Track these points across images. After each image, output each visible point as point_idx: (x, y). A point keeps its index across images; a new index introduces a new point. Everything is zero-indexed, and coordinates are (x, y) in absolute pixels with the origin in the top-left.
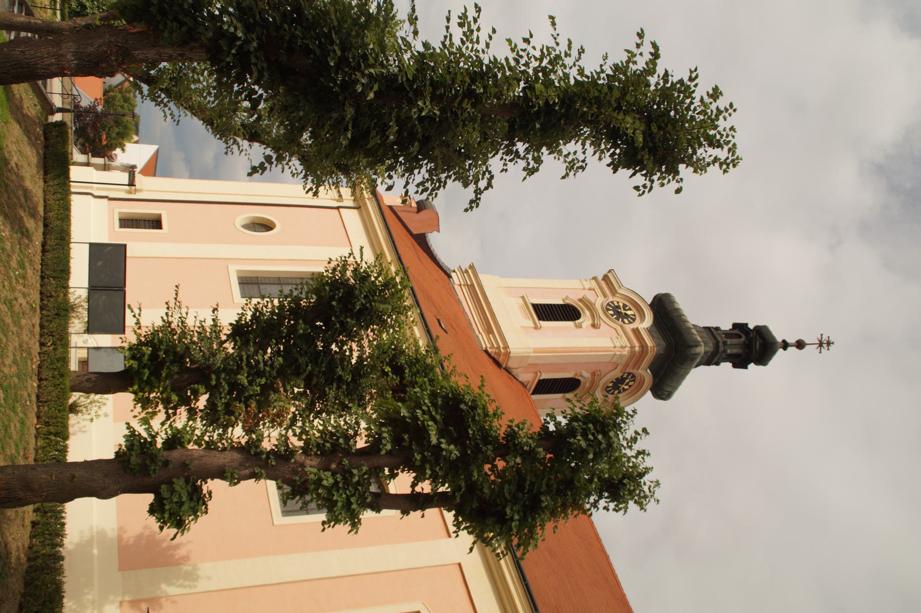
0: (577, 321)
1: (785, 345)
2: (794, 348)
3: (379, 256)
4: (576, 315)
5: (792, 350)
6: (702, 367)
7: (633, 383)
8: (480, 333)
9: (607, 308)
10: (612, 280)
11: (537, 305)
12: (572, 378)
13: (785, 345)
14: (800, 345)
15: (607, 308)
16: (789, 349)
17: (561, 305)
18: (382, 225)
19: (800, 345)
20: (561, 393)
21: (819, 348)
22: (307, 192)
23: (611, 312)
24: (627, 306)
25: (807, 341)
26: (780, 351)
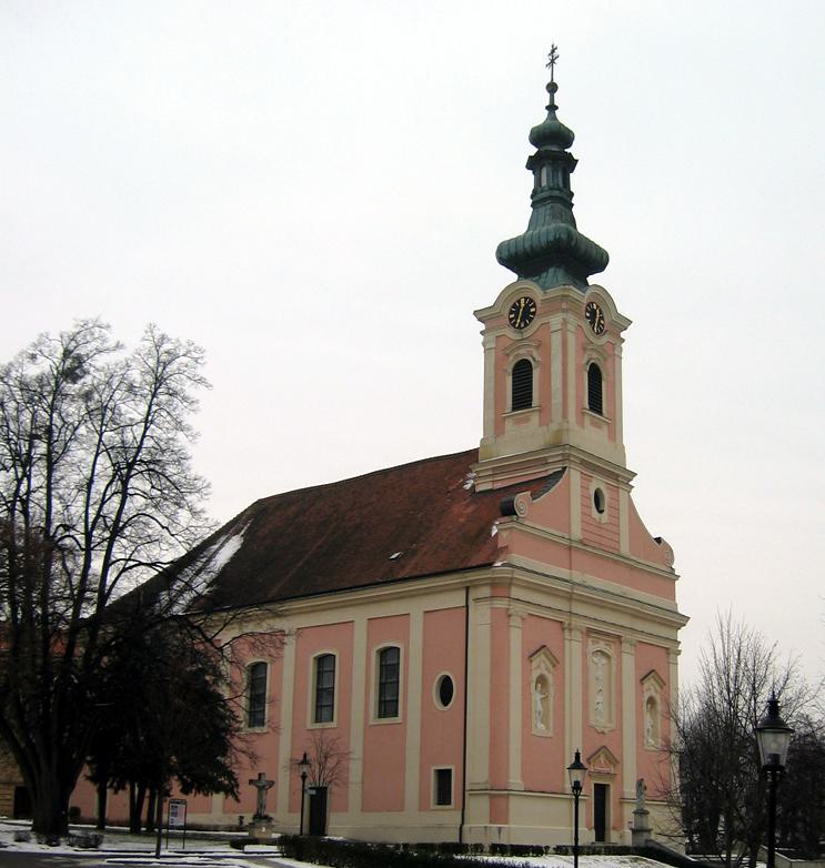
1: (552, 108)
13: (552, 108)
14: (552, 88)
18: (418, 582)
19: (552, 88)
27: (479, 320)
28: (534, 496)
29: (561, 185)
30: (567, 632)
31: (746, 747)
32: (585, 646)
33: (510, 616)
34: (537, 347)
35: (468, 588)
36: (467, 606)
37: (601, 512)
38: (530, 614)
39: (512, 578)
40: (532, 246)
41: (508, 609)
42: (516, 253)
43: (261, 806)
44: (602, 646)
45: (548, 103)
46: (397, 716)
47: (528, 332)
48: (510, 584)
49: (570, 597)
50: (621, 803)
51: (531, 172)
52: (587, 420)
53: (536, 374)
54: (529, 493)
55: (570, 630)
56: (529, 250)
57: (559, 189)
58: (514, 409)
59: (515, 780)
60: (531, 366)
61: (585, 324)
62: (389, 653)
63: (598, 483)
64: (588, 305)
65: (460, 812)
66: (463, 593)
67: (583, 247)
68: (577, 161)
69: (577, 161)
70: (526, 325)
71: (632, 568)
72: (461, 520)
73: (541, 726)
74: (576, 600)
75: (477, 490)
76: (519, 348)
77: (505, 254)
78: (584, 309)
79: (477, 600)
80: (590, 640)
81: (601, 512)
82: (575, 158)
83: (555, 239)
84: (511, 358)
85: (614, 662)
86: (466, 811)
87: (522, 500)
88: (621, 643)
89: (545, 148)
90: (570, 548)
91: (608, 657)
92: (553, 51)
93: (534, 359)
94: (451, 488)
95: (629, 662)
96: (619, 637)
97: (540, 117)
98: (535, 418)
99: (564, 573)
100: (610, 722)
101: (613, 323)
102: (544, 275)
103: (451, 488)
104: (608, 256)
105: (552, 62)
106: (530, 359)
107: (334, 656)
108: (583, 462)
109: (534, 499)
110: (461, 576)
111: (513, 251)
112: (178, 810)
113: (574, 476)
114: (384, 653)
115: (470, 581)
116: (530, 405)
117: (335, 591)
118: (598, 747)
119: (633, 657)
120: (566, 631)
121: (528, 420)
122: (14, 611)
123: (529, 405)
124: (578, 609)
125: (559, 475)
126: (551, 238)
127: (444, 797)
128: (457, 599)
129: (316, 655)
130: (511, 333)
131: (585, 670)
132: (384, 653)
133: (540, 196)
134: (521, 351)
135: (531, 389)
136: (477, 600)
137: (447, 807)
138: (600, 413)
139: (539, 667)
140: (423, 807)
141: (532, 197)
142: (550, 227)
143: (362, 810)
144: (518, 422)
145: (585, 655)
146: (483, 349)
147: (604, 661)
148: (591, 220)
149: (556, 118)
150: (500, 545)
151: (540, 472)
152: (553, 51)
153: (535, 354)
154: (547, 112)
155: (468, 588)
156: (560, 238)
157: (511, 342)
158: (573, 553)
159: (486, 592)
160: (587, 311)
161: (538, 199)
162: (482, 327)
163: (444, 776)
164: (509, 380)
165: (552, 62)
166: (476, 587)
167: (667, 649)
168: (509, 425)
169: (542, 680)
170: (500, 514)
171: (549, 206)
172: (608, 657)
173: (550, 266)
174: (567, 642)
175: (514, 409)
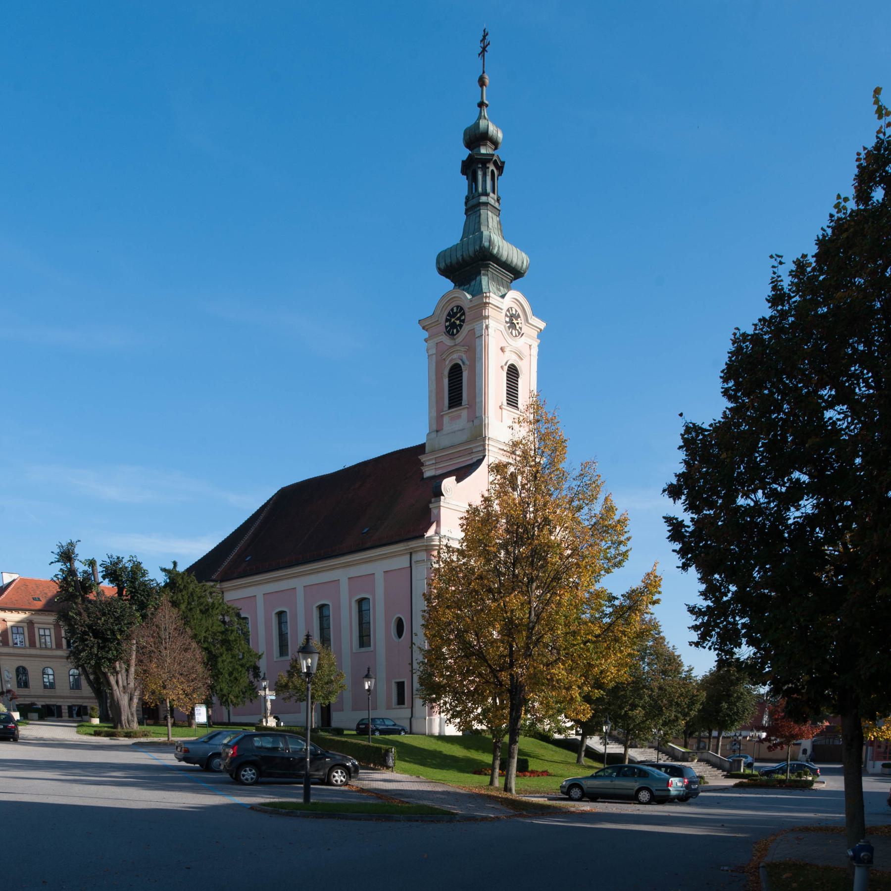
11: (449, 404)
23: (455, 331)
27: (424, 328)
28: (459, 480)
35: (411, 554)
36: (411, 567)
46: (370, 646)
47: (460, 338)
53: (465, 375)
54: (454, 478)
58: (450, 407)
62: (364, 602)
64: (508, 310)
65: (410, 709)
66: (408, 556)
70: (458, 332)
75: (425, 477)
77: (442, 265)
78: (504, 314)
86: (414, 709)
92: (484, 37)
93: (464, 363)
98: (464, 414)
105: (484, 49)
106: (461, 363)
110: (405, 544)
114: (361, 602)
117: (329, 557)
121: (459, 417)
122: (764, 503)
123: (460, 404)
127: (401, 701)
128: (404, 562)
129: (356, 599)
130: (447, 341)
132: (361, 602)
134: (455, 356)
135: (462, 390)
137: (403, 706)
141: (466, 203)
143: (343, 711)
148: (463, 181)
152: (484, 37)
153: (464, 357)
155: (411, 554)
160: (506, 315)
162: (426, 334)
163: (400, 686)
164: (446, 381)
165: (484, 49)
166: (416, 552)
168: (446, 419)
175: (450, 407)
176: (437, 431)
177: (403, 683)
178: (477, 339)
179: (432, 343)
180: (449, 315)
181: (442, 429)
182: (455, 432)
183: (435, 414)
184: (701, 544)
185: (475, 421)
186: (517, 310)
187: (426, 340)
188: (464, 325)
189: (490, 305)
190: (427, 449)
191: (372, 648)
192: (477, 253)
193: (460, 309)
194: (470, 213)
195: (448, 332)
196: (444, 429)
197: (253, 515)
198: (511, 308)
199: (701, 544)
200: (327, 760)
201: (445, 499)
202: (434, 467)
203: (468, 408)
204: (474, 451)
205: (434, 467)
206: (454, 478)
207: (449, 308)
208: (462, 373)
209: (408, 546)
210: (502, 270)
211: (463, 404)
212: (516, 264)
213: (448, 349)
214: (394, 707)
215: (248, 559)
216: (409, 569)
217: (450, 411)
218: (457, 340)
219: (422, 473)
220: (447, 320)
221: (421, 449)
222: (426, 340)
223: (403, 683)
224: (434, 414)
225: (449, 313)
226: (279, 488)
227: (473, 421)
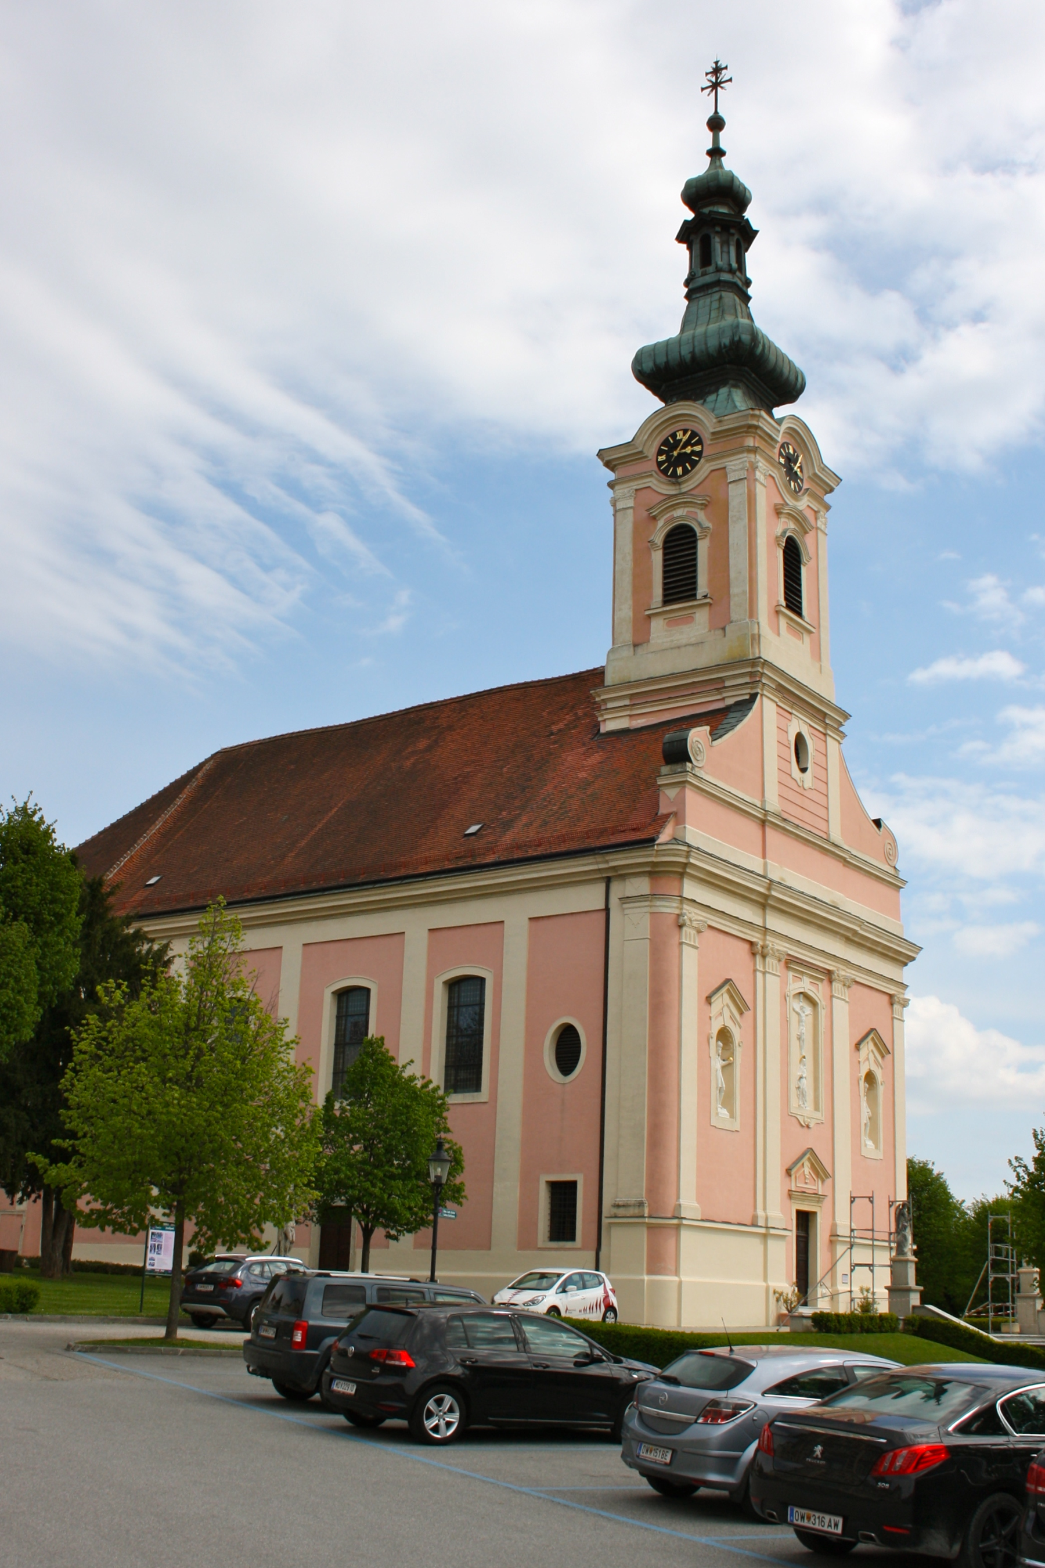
0: (698, 534)
1: (716, 153)
2: (722, 134)
3: (367, 1233)
4: (685, 532)
5: (725, 139)
6: (749, 255)
7: (790, 447)
8: (723, 699)
9: (671, 476)
10: (759, 541)
11: (665, 596)
12: (785, 552)
13: (716, 153)
14: (716, 124)
15: (671, 476)
16: (723, 145)
17: (665, 554)
18: (540, 866)
19: (716, 124)
20: (800, 568)
21: (722, 85)
22: (828, 508)
23: (680, 471)
24: (667, 439)
25: (711, 113)
26: (728, 163)
29: (735, 265)
30: (758, 958)
31: (227, 1229)
32: (784, 983)
33: (681, 927)
34: (704, 506)
36: (607, 910)
37: (804, 770)
38: (710, 927)
39: (686, 865)
40: (693, 353)
41: (678, 916)
42: (667, 363)
43: (634, 1205)
44: (805, 984)
45: (710, 146)
48: (682, 875)
49: (763, 903)
50: (831, 1242)
51: (685, 246)
52: (783, 622)
53: (703, 548)
54: (708, 728)
55: (764, 957)
56: (688, 357)
57: (731, 271)
58: (666, 602)
59: (689, 1203)
60: (695, 535)
61: (780, 474)
63: (798, 724)
65: (593, 1254)
66: (601, 887)
67: (772, 358)
68: (756, 232)
69: (756, 232)
70: (686, 472)
71: (846, 862)
72: (582, 775)
73: (724, 1112)
74: (774, 908)
75: (603, 730)
76: (674, 507)
77: (648, 366)
79: (625, 900)
80: (791, 974)
81: (804, 770)
82: (755, 228)
83: (732, 342)
84: (661, 523)
85: (823, 1013)
87: (697, 736)
88: (831, 981)
89: (706, 210)
90: (763, 823)
91: (813, 1003)
93: (700, 524)
94: (555, 728)
95: (841, 1011)
96: (829, 973)
97: (699, 167)
98: (702, 616)
99: (754, 863)
100: (817, 1108)
101: (815, 478)
102: (712, 398)
103: (555, 728)
104: (803, 379)
105: (715, 86)
107: (368, 990)
108: (781, 689)
109: (713, 740)
110: (599, 858)
111: (661, 360)
112: (163, 1241)
113: (767, 708)
114: (454, 985)
115: (614, 868)
116: (693, 597)
118: (804, 1148)
119: (889, 1269)
120: (758, 958)
121: (689, 619)
124: (776, 922)
125: (745, 705)
126: (726, 341)
128: (591, 897)
130: (664, 488)
131: (785, 1022)
132: (454, 985)
133: (700, 281)
134: (679, 512)
136: (625, 900)
137: (569, 1244)
138: (799, 614)
139: (721, 1014)
140: (526, 1242)
141: (687, 283)
142: (723, 323)
144: (672, 623)
145: (785, 997)
146: (611, 510)
147: (808, 1010)
149: (721, 167)
150: (663, 810)
151: (711, 702)
154: (708, 159)
156: (740, 340)
157: (663, 498)
158: (768, 830)
159: (641, 886)
160: (780, 454)
161: (695, 289)
164: (657, 558)
166: (623, 877)
167: (891, 996)
168: (657, 626)
169: (724, 1035)
170: (663, 762)
171: (716, 296)
172: (813, 1003)
173: (724, 383)
174: (759, 975)
176: (636, 645)
177: (572, 1185)
178: (730, 486)
179: (622, 490)
180: (665, 442)
181: (648, 641)
182: (679, 647)
183: (631, 614)
184: (83, 996)
185: (727, 629)
186: (796, 449)
187: (611, 485)
188: (702, 460)
189: (759, 432)
190: (609, 680)
191: (484, 1095)
192: (724, 351)
193: (695, 438)
194: (698, 295)
195: (665, 472)
196: (652, 642)
197: (155, 799)
198: (788, 444)
199: (83, 996)
200: (350, 1389)
201: (693, 768)
202: (628, 713)
203: (710, 604)
204: (727, 684)
205: (628, 713)
206: (708, 728)
207: (666, 433)
208: (695, 542)
209: (607, 862)
210: (762, 384)
211: (699, 597)
212: (788, 378)
213: (665, 500)
214: (540, 1244)
215: (152, 881)
216: (603, 915)
217: (665, 609)
218: (682, 486)
219: (597, 725)
220: (660, 452)
221: (596, 676)
222: (611, 485)
223: (572, 1185)
224: (627, 611)
225: (667, 440)
226: (218, 749)
227: (724, 629)
